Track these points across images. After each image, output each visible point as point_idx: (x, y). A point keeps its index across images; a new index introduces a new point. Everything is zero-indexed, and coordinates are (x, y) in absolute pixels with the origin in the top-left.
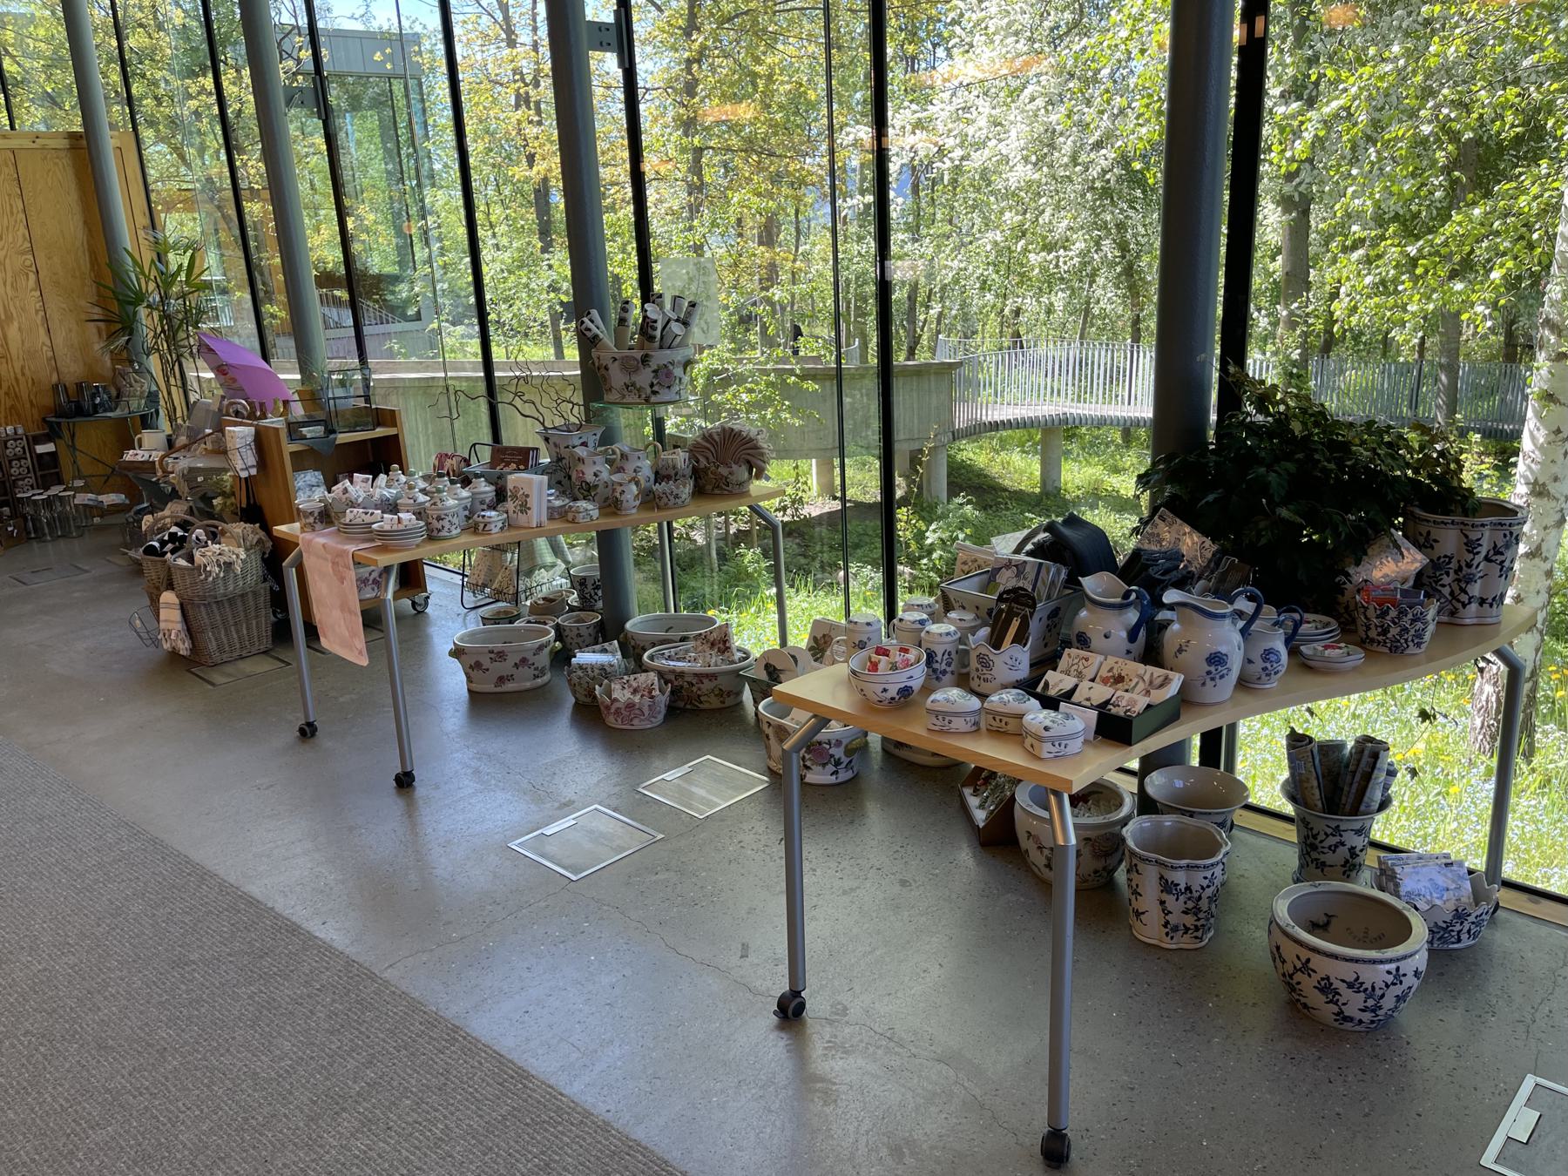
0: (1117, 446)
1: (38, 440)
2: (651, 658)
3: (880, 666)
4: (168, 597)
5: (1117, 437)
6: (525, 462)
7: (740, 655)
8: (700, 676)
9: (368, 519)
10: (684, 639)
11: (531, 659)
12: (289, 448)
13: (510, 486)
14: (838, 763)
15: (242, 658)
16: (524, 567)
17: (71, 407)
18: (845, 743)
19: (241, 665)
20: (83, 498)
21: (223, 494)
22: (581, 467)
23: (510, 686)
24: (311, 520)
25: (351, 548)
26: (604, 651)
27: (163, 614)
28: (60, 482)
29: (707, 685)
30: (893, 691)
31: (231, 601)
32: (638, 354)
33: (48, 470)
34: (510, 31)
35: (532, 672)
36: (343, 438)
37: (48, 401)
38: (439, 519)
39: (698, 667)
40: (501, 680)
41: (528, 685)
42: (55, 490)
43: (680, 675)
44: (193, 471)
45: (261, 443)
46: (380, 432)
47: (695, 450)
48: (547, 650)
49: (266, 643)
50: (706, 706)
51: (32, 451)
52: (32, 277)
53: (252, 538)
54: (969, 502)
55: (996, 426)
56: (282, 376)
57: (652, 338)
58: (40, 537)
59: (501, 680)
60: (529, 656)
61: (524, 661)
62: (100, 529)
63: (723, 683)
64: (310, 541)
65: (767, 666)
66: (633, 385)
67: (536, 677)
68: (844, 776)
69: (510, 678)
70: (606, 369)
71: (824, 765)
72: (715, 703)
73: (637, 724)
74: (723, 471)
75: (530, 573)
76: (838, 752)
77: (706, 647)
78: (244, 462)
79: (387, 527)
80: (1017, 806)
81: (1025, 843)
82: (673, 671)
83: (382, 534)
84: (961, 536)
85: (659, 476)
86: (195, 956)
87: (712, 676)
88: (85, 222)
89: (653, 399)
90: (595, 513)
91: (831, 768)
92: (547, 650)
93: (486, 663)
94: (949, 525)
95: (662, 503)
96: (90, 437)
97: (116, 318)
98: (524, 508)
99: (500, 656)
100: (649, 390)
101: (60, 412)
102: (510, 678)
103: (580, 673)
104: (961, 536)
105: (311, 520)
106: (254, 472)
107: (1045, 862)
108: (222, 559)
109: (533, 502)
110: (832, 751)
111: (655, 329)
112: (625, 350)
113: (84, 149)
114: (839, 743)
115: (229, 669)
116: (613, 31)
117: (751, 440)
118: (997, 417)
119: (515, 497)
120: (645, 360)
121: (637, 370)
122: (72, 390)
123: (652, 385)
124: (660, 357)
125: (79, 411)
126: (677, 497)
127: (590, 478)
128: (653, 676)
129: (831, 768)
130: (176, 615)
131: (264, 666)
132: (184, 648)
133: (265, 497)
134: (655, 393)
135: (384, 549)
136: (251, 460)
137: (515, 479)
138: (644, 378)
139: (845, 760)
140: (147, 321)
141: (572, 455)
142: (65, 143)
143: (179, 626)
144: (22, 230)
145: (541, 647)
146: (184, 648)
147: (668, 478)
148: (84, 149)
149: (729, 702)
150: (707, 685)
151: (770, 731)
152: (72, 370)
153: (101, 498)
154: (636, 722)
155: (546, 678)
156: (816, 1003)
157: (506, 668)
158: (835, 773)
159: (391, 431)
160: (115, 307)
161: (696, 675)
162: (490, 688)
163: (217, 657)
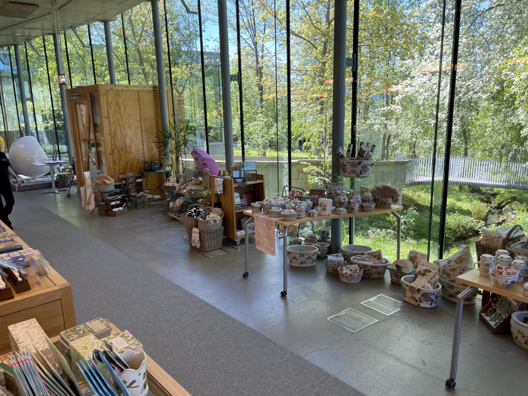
0: (457, 192)
1: (137, 178)
2: (353, 259)
3: (503, 273)
4: (195, 230)
5: (457, 188)
6: (321, 194)
7: (384, 261)
8: (372, 267)
9: (278, 211)
10: (362, 254)
11: (312, 257)
12: (235, 185)
13: (320, 202)
14: (432, 301)
15: (214, 250)
16: (301, 226)
17: (150, 167)
18: (436, 294)
19: (215, 252)
20: (149, 196)
21: (202, 198)
22: (339, 197)
23: (303, 265)
24: (257, 210)
25: (275, 219)
26: (337, 256)
27: (193, 235)
28: (142, 191)
29: (375, 270)
30: (509, 282)
31: (214, 232)
32: (357, 161)
33: (139, 187)
34: (256, 52)
35: (311, 261)
36: (249, 183)
37: (142, 166)
38: (300, 212)
39: (371, 264)
40: (302, 263)
41: (309, 265)
42: (141, 193)
43: (365, 266)
44: (191, 190)
45: (224, 184)
46: (258, 181)
47: (373, 192)
48: (316, 254)
49: (221, 246)
50: (373, 277)
51: (135, 181)
52: (140, 128)
53: (220, 213)
54: (415, 209)
55: (419, 183)
56: (216, 161)
57: (362, 156)
58: (136, 207)
59: (302, 263)
60: (311, 256)
61: (310, 257)
62: (153, 206)
63: (380, 270)
64: (258, 216)
65: (397, 266)
66: (354, 171)
67: (313, 263)
68: (434, 305)
69: (305, 262)
70: (345, 165)
71: (428, 301)
72: (376, 276)
73: (353, 281)
74: (384, 200)
75: (302, 228)
76: (433, 297)
77: (372, 257)
78: (219, 190)
79: (286, 214)
80: (512, 321)
81: (515, 334)
82: (363, 265)
83: (284, 216)
84: (411, 221)
85: (363, 201)
86: (242, 346)
87: (377, 267)
88: (156, 113)
89: (360, 175)
90: (346, 212)
91: (430, 302)
92: (316, 254)
93: (298, 257)
94: (408, 217)
95: (365, 210)
96: (152, 177)
97: (162, 142)
98: (324, 209)
99: (303, 255)
100: (359, 173)
101: (146, 170)
102: (305, 262)
103: (331, 263)
104: (411, 221)
105: (257, 210)
106: (222, 192)
107: (524, 341)
108: (215, 219)
109: (327, 208)
110: (431, 297)
111: (364, 153)
112: (349, 158)
113: (157, 92)
114: (434, 294)
115: (210, 253)
116: (352, 60)
117: (394, 190)
118: (420, 180)
119: (321, 206)
120: (359, 163)
121: (356, 166)
122: (149, 163)
123: (361, 171)
124: (365, 162)
125: (151, 170)
126: (371, 208)
127: (342, 200)
128: (357, 266)
129: (430, 302)
130: (198, 235)
131: (221, 253)
132: (198, 246)
133: (223, 200)
134: (361, 174)
135: (284, 220)
136: (222, 189)
137: (321, 200)
138: (359, 168)
139: (435, 300)
140: (172, 144)
141: (336, 193)
142: (151, 89)
143: (198, 239)
144: (139, 115)
145: (315, 253)
146: (198, 246)
147: (366, 201)
148: (157, 92)
149: (381, 276)
150: (375, 270)
151: (407, 288)
152: (147, 158)
153: (155, 196)
154: (352, 281)
155: (315, 263)
156: (458, 381)
157: (303, 259)
158: (431, 304)
159: (261, 181)
160: (162, 138)
161: (371, 266)
162: (298, 265)
163: (208, 249)
